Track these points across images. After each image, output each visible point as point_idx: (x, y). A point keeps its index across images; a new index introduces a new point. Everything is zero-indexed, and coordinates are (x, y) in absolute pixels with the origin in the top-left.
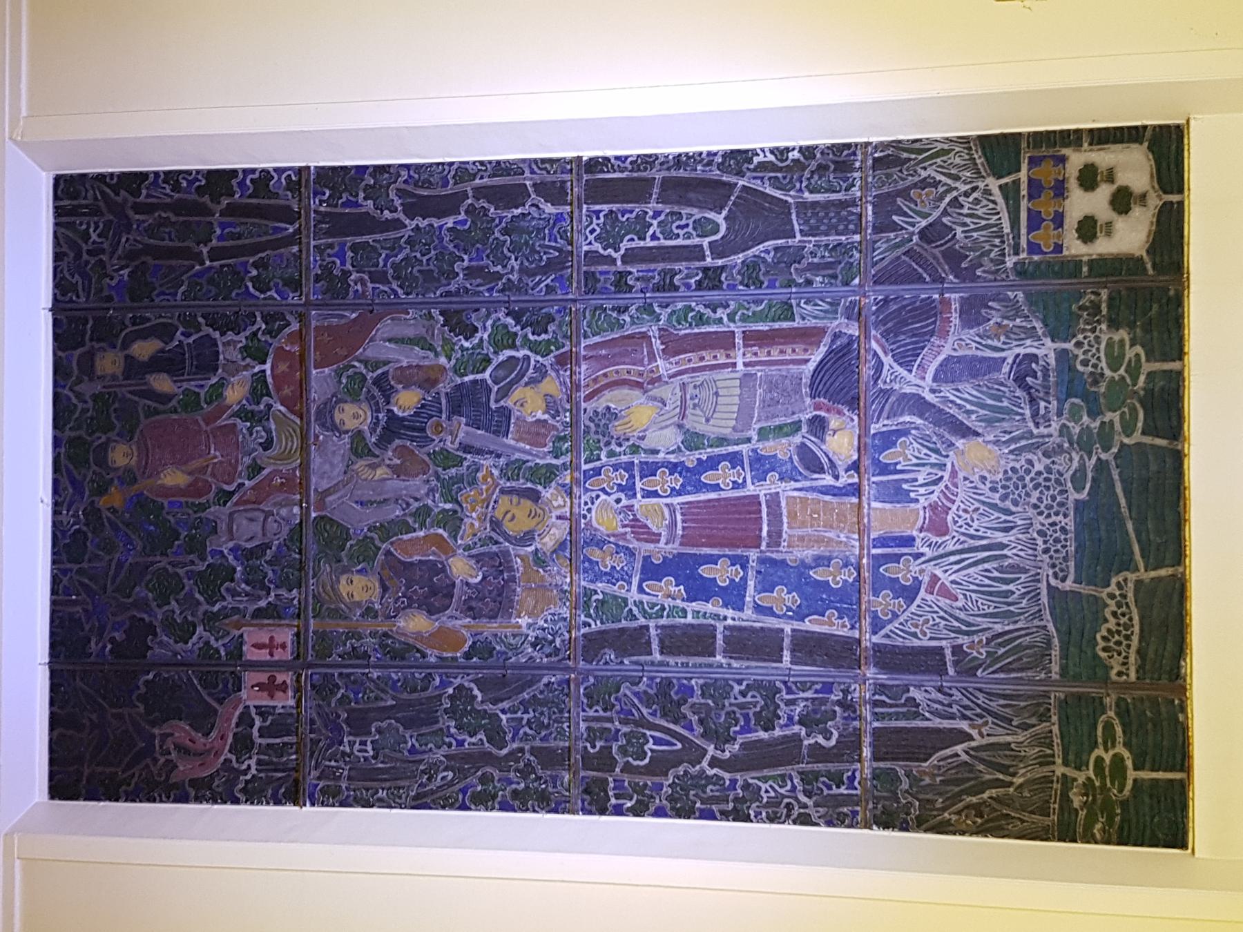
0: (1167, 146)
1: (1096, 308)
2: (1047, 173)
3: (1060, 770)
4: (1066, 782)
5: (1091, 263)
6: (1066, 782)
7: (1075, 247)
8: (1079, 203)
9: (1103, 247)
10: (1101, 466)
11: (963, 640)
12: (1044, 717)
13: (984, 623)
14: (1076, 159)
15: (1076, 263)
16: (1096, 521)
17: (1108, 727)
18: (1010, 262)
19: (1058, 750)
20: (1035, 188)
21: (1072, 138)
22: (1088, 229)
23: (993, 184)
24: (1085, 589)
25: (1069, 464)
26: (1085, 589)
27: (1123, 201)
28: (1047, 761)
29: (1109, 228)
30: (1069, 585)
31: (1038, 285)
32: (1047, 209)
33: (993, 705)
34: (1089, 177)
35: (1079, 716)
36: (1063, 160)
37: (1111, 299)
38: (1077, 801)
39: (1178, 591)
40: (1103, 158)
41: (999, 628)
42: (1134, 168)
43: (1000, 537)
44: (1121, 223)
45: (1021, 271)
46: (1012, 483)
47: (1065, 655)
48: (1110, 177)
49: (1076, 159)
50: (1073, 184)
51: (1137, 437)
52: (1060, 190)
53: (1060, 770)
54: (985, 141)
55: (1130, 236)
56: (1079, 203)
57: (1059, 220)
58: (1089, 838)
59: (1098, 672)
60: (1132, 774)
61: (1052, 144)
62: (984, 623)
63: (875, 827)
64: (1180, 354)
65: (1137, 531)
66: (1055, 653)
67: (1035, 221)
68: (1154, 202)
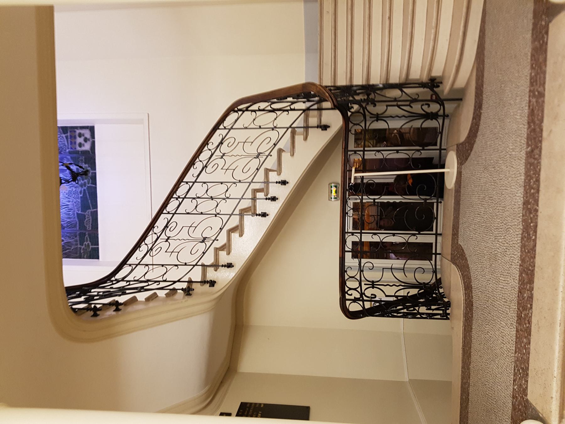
0: (92, 129)
1: (82, 160)
2: (73, 134)
3: (79, 246)
4: (80, 248)
5: (81, 152)
6: (80, 248)
7: (78, 149)
8: (79, 140)
9: (83, 148)
10: (84, 190)
11: (62, 223)
12: (76, 237)
13: (66, 219)
14: (78, 131)
15: (78, 151)
16: (84, 199)
17: (87, 238)
18: (67, 150)
19: (79, 243)
20: (71, 136)
21: (76, 128)
22: (80, 145)
23: (64, 136)
24: (83, 213)
25: (79, 189)
26: (83, 213)
27: (86, 140)
28: (77, 245)
29: (84, 145)
30: (80, 212)
31: (72, 155)
32: (73, 141)
33: (68, 235)
34: (80, 135)
35: (82, 236)
36: (75, 132)
37: (85, 158)
38: (82, 251)
39: (96, 213)
40: (82, 131)
41: (68, 220)
42: (87, 134)
43: (68, 203)
44: (86, 144)
45: (70, 152)
46: (70, 192)
47: (80, 225)
48: (83, 136)
49: (78, 131)
50: (77, 136)
51: (90, 185)
52: (75, 138)
53: (79, 246)
54: (90, 157)
55: (87, 147)
56: (79, 140)
57: (75, 143)
58: (84, 258)
59: (85, 228)
60: (91, 247)
61: (73, 129)
62: (66, 219)
63: (392, 255)
64: (95, 170)
65: (91, 202)
66: (78, 225)
67: (71, 143)
68: (91, 140)
